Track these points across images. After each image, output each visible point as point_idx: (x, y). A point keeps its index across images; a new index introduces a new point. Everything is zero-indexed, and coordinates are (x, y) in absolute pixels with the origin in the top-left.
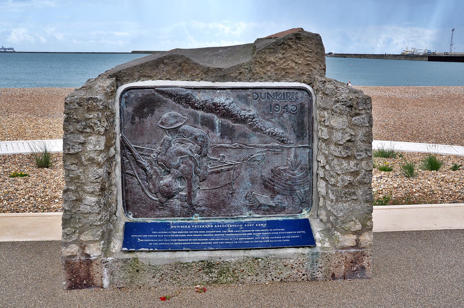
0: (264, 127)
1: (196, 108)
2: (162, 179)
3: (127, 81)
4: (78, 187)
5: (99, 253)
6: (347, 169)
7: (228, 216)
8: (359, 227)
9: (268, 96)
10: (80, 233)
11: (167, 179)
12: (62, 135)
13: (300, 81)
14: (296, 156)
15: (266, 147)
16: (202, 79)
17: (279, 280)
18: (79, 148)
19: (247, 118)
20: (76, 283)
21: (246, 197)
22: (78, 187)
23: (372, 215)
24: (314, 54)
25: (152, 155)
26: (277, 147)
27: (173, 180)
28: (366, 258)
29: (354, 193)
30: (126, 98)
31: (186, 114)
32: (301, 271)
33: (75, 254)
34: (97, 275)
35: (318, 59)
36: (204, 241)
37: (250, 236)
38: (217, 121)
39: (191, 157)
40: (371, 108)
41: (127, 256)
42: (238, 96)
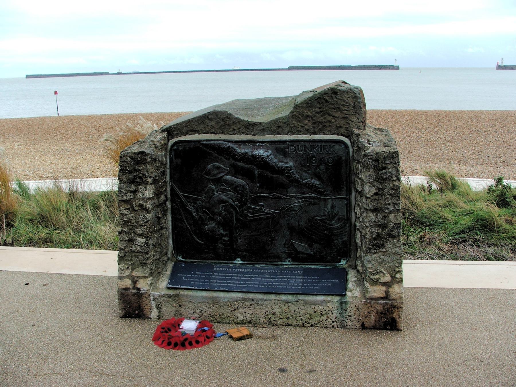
0: (301, 178)
1: (236, 160)
2: (207, 225)
3: (177, 135)
4: (130, 229)
5: (148, 288)
6: (375, 221)
7: (268, 262)
8: (387, 278)
9: (305, 149)
10: (133, 269)
11: (212, 225)
12: (368, 115)
13: (338, 135)
14: (333, 207)
15: (303, 197)
16: (243, 133)
17: (309, 325)
18: (131, 196)
19: (284, 170)
20: (129, 313)
21: (285, 244)
22: (130, 229)
23: (401, 268)
24: (351, 108)
25: (198, 202)
26: (314, 198)
27: (217, 227)
28: (396, 309)
29: (383, 246)
30: (175, 150)
31: (227, 166)
32: (331, 318)
33: (128, 287)
34: (146, 307)
35: (355, 112)
36: (241, 284)
37: (285, 282)
38: (257, 172)
39: (232, 206)
40: (399, 162)
41: (171, 292)
42: (276, 149)
